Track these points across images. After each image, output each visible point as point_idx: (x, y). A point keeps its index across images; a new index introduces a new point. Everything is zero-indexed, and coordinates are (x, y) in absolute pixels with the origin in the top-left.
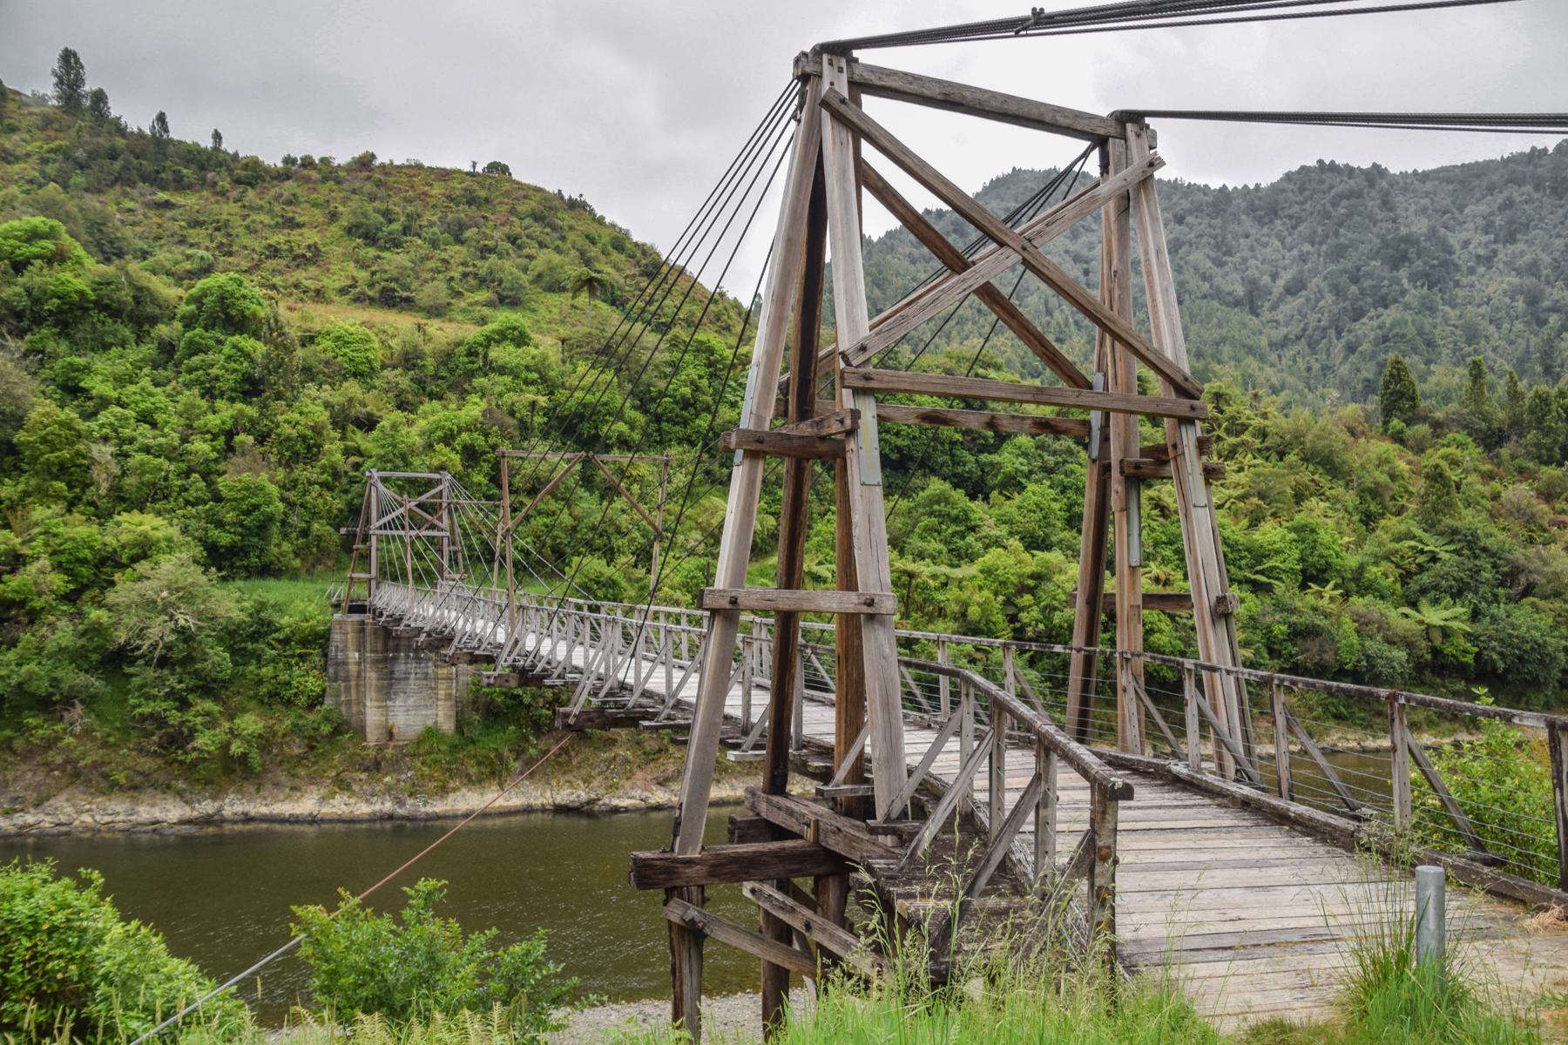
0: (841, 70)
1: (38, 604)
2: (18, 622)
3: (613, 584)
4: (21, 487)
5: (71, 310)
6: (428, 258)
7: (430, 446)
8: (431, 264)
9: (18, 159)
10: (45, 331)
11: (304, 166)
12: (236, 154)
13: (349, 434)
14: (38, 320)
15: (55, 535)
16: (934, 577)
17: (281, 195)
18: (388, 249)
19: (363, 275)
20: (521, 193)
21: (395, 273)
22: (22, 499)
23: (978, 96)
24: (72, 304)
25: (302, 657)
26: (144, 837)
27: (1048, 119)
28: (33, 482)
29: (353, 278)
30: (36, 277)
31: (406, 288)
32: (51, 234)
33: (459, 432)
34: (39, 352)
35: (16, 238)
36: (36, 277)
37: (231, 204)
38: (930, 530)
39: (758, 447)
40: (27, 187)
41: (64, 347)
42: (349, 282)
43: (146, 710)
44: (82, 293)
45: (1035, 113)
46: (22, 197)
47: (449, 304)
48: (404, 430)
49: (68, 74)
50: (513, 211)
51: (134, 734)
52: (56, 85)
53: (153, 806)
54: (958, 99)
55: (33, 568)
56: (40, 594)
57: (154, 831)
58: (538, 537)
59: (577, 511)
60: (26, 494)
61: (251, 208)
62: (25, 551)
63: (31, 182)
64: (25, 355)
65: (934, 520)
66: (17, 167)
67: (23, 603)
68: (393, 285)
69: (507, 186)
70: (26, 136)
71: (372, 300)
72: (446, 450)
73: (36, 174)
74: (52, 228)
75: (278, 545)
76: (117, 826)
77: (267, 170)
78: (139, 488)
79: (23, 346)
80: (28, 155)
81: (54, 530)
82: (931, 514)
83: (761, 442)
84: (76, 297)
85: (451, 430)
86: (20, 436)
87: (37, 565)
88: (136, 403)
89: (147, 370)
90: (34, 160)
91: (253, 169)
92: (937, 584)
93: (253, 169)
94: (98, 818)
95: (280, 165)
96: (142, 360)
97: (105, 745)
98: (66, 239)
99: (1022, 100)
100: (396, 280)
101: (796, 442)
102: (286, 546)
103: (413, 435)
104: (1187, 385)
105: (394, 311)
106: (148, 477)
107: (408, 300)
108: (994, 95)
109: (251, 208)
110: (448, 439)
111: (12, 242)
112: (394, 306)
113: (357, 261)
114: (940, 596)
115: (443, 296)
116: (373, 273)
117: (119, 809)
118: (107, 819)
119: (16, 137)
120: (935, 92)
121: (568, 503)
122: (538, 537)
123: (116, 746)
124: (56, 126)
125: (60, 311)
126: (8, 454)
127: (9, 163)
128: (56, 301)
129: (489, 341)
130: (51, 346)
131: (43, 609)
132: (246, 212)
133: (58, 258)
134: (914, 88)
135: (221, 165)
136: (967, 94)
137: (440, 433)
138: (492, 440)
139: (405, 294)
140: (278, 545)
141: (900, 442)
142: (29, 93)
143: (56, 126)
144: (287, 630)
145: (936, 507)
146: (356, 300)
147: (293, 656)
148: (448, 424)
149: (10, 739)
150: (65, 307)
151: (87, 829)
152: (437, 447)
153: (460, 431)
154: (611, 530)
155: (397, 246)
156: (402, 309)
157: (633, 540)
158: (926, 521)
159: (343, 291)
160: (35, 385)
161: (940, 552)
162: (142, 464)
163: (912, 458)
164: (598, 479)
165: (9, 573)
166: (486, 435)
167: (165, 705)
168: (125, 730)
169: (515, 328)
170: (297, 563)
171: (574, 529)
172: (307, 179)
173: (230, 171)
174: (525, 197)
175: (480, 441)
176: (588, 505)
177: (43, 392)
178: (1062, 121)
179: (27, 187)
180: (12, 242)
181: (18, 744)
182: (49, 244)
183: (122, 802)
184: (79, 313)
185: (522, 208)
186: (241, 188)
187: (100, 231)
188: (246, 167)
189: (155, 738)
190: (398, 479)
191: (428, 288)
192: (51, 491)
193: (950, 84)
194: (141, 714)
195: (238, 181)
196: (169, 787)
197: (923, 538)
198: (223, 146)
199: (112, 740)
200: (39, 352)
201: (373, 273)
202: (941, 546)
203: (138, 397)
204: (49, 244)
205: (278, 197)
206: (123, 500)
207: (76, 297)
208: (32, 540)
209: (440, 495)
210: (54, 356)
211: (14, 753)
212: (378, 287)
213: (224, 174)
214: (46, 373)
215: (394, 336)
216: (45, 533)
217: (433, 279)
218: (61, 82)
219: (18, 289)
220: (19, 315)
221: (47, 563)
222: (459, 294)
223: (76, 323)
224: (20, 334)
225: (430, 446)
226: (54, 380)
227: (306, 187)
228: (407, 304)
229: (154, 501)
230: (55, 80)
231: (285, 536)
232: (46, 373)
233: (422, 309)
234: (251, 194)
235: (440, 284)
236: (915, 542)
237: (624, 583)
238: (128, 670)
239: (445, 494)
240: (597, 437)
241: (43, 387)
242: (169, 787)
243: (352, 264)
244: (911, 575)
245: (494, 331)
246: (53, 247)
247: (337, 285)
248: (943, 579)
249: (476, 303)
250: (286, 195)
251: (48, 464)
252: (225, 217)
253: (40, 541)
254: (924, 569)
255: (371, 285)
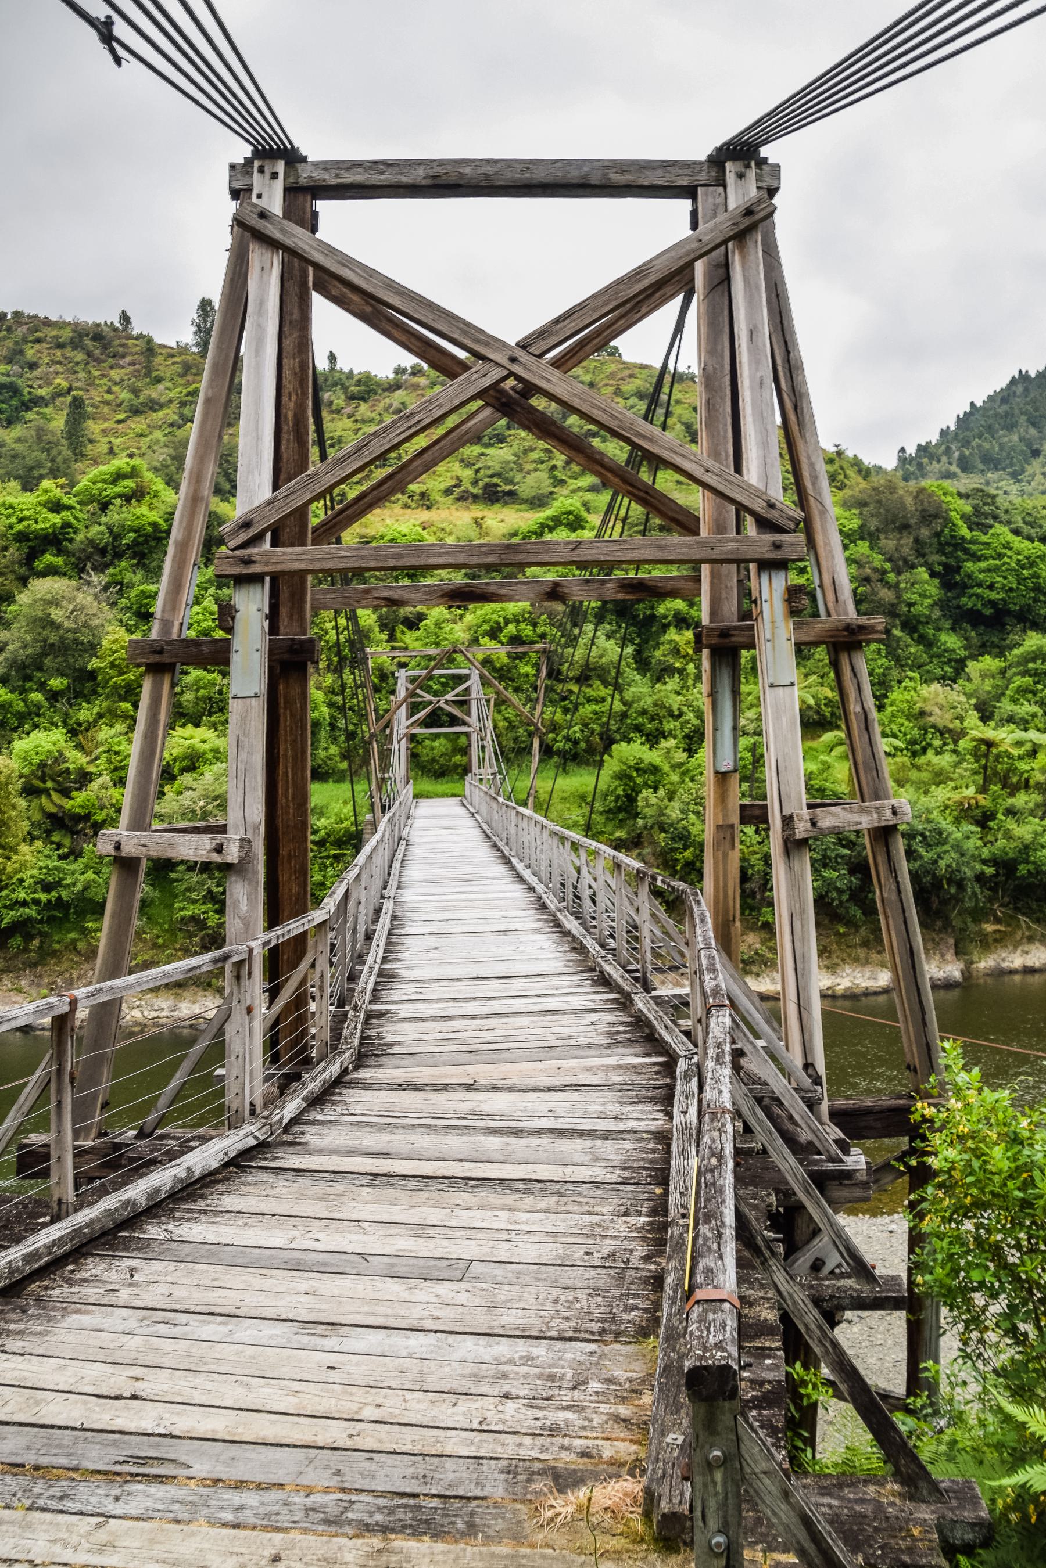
0: (274, 176)
1: (99, 817)
2: (86, 835)
3: (655, 769)
4: (96, 710)
5: (146, 542)
6: (532, 450)
7: (475, 641)
8: (534, 456)
9: (162, 406)
10: (123, 564)
11: (413, 374)
12: (351, 371)
13: (398, 635)
14: (118, 555)
15: (117, 753)
16: (1019, 744)
17: (391, 405)
18: (492, 445)
19: (467, 474)
20: (627, 372)
21: (497, 468)
22: (96, 721)
23: (486, 169)
24: (146, 535)
25: (336, 858)
26: (186, 1031)
27: (595, 180)
28: (104, 704)
29: (458, 478)
30: (115, 516)
31: (509, 481)
32: (134, 473)
33: (507, 624)
34: (117, 583)
35: (104, 481)
36: (115, 516)
37: (346, 420)
38: (1023, 691)
39: (157, 658)
40: (168, 430)
41: (139, 576)
42: (454, 482)
43: (187, 913)
44: (155, 525)
45: (558, 175)
46: (163, 439)
47: (551, 493)
48: (447, 627)
49: (206, 321)
50: (618, 392)
51: (180, 935)
52: (195, 333)
53: (194, 1002)
54: (453, 179)
55: (95, 785)
56: (102, 808)
57: (191, 1026)
58: (586, 725)
59: (628, 695)
60: (100, 716)
61: (363, 421)
62: (92, 769)
63: (172, 425)
64: (106, 588)
65: (1028, 680)
66: (161, 414)
67: (87, 817)
68: (495, 480)
69: (612, 367)
70: (169, 384)
71: (475, 498)
72: (493, 644)
73: (176, 417)
74: (134, 468)
75: (326, 749)
76: (161, 1021)
77: (378, 384)
78: (197, 704)
79: (104, 579)
80: (170, 401)
81: (116, 748)
82: (1026, 673)
83: (160, 652)
84: (149, 529)
85: (498, 623)
86: (94, 664)
87: (100, 780)
88: (199, 623)
89: (212, 591)
90: (174, 406)
91: (366, 384)
92: (1021, 751)
93: (366, 384)
94: (146, 1013)
95: (391, 376)
96: (208, 581)
97: (155, 946)
98: (148, 475)
99: (554, 162)
100: (498, 475)
101: (205, 648)
102: (334, 750)
103: (459, 632)
104: (772, 515)
105: (497, 506)
106: (202, 692)
107: (511, 494)
108: (509, 163)
109: (363, 421)
110: (494, 633)
111: (100, 485)
112: (497, 501)
113: (462, 461)
114: (1023, 766)
115: (546, 486)
116: (477, 471)
117: (164, 1005)
118: (154, 1014)
119: (161, 387)
120: (418, 176)
121: (618, 688)
122: (586, 725)
123: (164, 947)
124: (194, 371)
125: (135, 543)
126: (88, 680)
127: (155, 411)
128: (132, 535)
129: (544, 527)
130: (128, 576)
131: (104, 821)
132: (359, 426)
133: (137, 495)
134: (389, 177)
135: (335, 384)
136: (467, 170)
137: (486, 627)
138: (540, 629)
139: (508, 488)
140: (326, 749)
141: (994, 595)
142: (174, 345)
143: (194, 371)
144: (323, 833)
145: (1031, 665)
146: (461, 499)
147: (328, 857)
148: (495, 617)
149: (74, 942)
150: (141, 539)
151: (137, 1024)
152: (482, 641)
153: (507, 622)
154: (663, 713)
155: (501, 441)
156: (506, 503)
157: (688, 721)
158: (1019, 681)
159: (448, 492)
160: (110, 614)
161: (1034, 715)
162: (198, 680)
163: (1009, 612)
164: (653, 661)
165: (77, 789)
166: (535, 625)
167: (204, 908)
168: (172, 932)
169: (570, 513)
170: (344, 766)
171: (624, 715)
172: (416, 387)
173: (345, 388)
174: (631, 376)
175: (527, 630)
176: (639, 688)
177: (121, 621)
178: (617, 178)
179: (168, 430)
180: (100, 485)
181: (81, 945)
182: (130, 483)
183: (167, 999)
184: (153, 543)
185: (627, 388)
186: (354, 403)
187: (227, 461)
188: (359, 383)
189: (197, 939)
190: (441, 676)
191: (530, 480)
192: (119, 712)
193: (441, 162)
194: (183, 918)
195: (352, 398)
196: (209, 985)
197: (1015, 701)
198: (338, 367)
199: (160, 941)
200: (117, 583)
201: (477, 471)
202: (1035, 709)
203: (201, 617)
204: (130, 483)
205: (387, 409)
206: (182, 715)
207: (149, 529)
208: (97, 758)
209: (467, 691)
210: (131, 586)
211: (79, 953)
212: (481, 484)
213: (340, 392)
214: (123, 602)
215: (450, 534)
216: (109, 751)
217: (536, 470)
218: (199, 330)
219: (102, 528)
220: (103, 552)
221: (108, 779)
222: (562, 482)
223: (151, 552)
224: (100, 569)
225: (475, 641)
226: (130, 608)
227: (415, 394)
228: (511, 497)
229: (210, 715)
230: (194, 329)
231: (335, 739)
232: (123, 602)
233: (525, 501)
234: (364, 407)
235: (543, 475)
236: (1006, 706)
237: (666, 768)
238: (173, 875)
239: (474, 690)
240: (653, 617)
241: (119, 616)
242: (209, 985)
243: (457, 464)
244: (989, 744)
245: (548, 518)
246: (133, 485)
247: (443, 486)
248: (1028, 746)
249: (579, 489)
250: (396, 404)
251: (116, 687)
252: (338, 433)
253: (103, 758)
254: (1005, 736)
255: (475, 483)
